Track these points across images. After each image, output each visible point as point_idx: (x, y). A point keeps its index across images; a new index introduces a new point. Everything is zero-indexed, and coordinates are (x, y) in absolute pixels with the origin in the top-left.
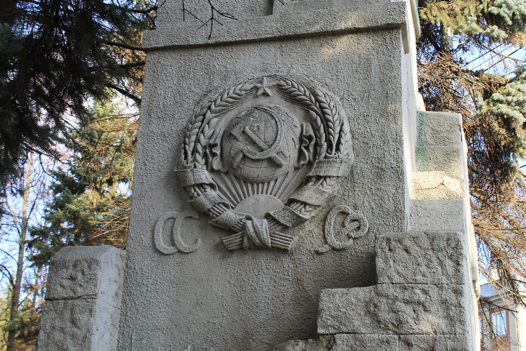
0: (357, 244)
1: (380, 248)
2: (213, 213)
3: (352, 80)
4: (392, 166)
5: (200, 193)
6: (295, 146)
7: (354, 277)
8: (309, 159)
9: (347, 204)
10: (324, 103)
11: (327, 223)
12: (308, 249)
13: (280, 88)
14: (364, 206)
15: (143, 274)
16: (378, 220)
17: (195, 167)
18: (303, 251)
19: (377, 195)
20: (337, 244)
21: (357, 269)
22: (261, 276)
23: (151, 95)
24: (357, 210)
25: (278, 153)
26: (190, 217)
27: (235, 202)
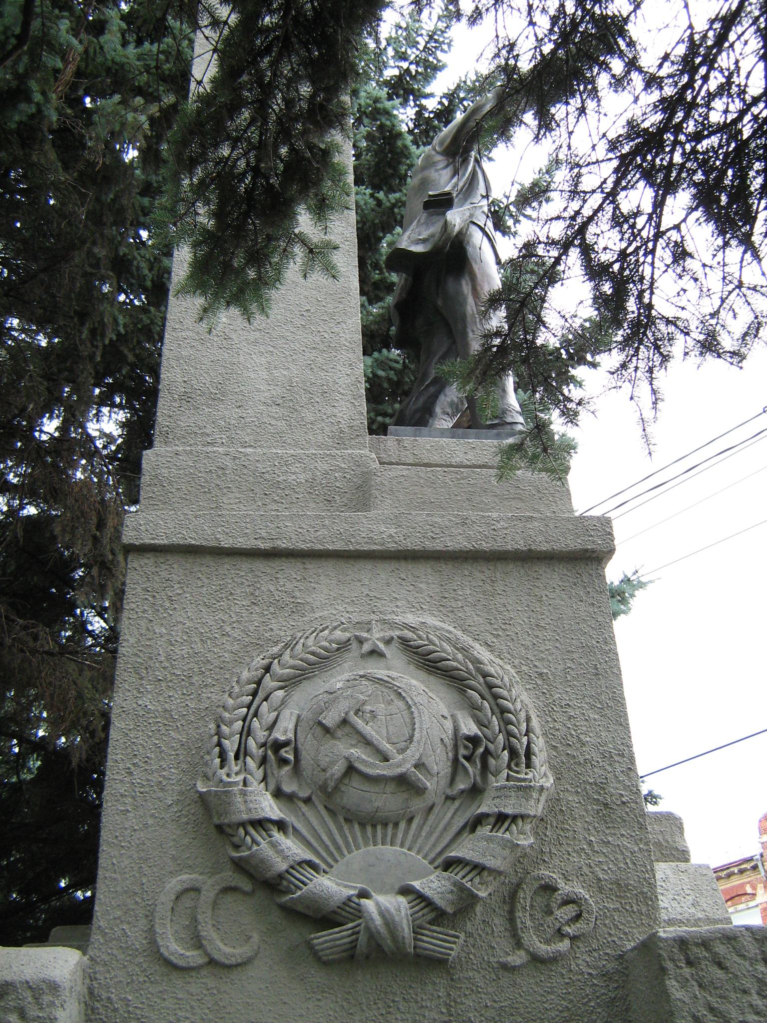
0: (579, 948)
2: (291, 882)
4: (623, 799)
5: (259, 839)
7: (579, 1015)
10: (493, 677)
12: (486, 958)
14: (582, 875)
15: (129, 1012)
17: (245, 783)
20: (544, 949)
21: (583, 998)
22: (394, 1017)
27: (330, 860)
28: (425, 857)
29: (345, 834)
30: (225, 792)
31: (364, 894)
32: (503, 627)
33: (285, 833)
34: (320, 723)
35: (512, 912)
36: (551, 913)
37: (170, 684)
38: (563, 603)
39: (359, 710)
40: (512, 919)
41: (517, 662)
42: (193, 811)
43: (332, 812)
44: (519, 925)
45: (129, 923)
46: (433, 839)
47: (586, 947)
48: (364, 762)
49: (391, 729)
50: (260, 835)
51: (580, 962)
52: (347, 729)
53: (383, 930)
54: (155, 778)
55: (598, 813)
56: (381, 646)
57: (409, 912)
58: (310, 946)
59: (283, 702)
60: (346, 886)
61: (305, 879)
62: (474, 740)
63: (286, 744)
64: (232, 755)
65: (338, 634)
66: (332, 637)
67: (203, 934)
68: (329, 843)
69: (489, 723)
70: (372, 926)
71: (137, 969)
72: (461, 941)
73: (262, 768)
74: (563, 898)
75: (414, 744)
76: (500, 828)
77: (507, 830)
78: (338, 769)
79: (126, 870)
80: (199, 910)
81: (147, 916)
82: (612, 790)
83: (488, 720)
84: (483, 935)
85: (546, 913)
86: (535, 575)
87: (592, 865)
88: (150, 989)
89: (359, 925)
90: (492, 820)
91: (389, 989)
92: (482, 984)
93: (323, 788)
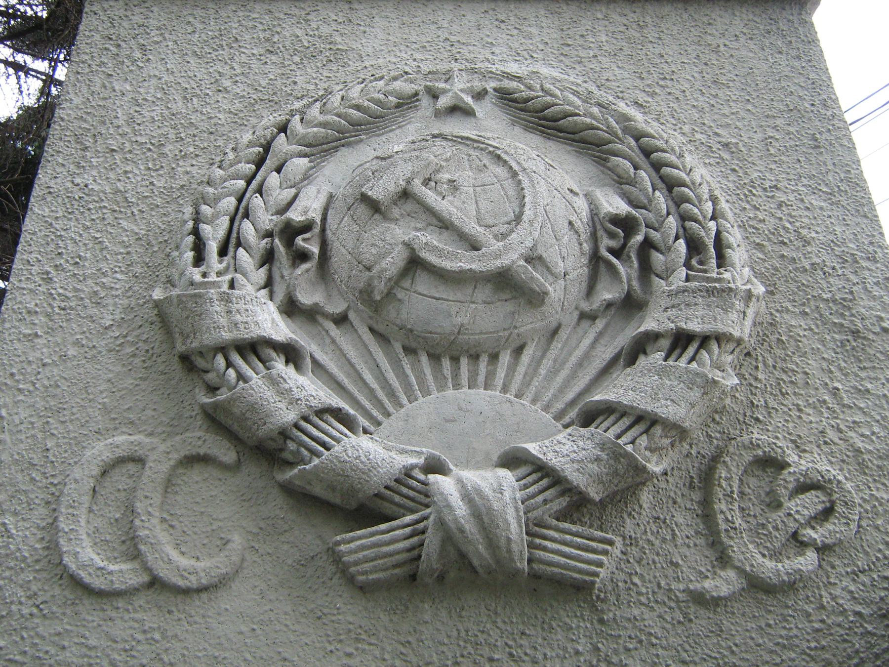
0: (833, 567)
2: (302, 444)
5: (249, 372)
6: (581, 244)
8: (630, 285)
9: (770, 434)
12: (663, 583)
13: (506, 98)
14: (826, 443)
17: (232, 285)
18: (644, 590)
19: (860, 409)
21: (850, 657)
24: (807, 455)
25: (528, 260)
26: (203, 460)
27: (375, 413)
28: (546, 408)
29: (404, 373)
30: (195, 295)
31: (435, 467)
32: (661, 83)
33: (298, 368)
34: (365, 198)
35: (706, 503)
36: (779, 505)
37: (128, 156)
38: (752, 55)
39: (430, 179)
40: (707, 515)
41: (686, 128)
42: (145, 336)
43: (382, 338)
44: (723, 526)
45: (15, 514)
46: (559, 379)
47: (848, 565)
48: (434, 249)
49: (483, 205)
50: (253, 369)
51: (838, 592)
52: (409, 206)
53: (470, 527)
54: (89, 286)
55: (843, 345)
56: (468, 100)
57: (518, 495)
58: (336, 558)
59: (307, 177)
60: (403, 452)
61: (327, 439)
62: (626, 224)
63: (306, 227)
64: (213, 247)
65: (398, 85)
66: (390, 88)
67: (142, 533)
68: (375, 385)
69: (650, 201)
70: (448, 518)
71: (21, 593)
72: (616, 551)
73: (266, 267)
74: (797, 480)
75: (525, 224)
76: (680, 356)
77: (693, 359)
78: (393, 262)
79: (21, 427)
80: (140, 494)
81: (48, 503)
82: (863, 311)
83: (647, 195)
84: (657, 543)
85: (768, 505)
86: (705, 19)
87: (842, 427)
88: (40, 630)
89: (426, 518)
90: (665, 343)
91: (481, 638)
92: (656, 630)
93: (366, 294)
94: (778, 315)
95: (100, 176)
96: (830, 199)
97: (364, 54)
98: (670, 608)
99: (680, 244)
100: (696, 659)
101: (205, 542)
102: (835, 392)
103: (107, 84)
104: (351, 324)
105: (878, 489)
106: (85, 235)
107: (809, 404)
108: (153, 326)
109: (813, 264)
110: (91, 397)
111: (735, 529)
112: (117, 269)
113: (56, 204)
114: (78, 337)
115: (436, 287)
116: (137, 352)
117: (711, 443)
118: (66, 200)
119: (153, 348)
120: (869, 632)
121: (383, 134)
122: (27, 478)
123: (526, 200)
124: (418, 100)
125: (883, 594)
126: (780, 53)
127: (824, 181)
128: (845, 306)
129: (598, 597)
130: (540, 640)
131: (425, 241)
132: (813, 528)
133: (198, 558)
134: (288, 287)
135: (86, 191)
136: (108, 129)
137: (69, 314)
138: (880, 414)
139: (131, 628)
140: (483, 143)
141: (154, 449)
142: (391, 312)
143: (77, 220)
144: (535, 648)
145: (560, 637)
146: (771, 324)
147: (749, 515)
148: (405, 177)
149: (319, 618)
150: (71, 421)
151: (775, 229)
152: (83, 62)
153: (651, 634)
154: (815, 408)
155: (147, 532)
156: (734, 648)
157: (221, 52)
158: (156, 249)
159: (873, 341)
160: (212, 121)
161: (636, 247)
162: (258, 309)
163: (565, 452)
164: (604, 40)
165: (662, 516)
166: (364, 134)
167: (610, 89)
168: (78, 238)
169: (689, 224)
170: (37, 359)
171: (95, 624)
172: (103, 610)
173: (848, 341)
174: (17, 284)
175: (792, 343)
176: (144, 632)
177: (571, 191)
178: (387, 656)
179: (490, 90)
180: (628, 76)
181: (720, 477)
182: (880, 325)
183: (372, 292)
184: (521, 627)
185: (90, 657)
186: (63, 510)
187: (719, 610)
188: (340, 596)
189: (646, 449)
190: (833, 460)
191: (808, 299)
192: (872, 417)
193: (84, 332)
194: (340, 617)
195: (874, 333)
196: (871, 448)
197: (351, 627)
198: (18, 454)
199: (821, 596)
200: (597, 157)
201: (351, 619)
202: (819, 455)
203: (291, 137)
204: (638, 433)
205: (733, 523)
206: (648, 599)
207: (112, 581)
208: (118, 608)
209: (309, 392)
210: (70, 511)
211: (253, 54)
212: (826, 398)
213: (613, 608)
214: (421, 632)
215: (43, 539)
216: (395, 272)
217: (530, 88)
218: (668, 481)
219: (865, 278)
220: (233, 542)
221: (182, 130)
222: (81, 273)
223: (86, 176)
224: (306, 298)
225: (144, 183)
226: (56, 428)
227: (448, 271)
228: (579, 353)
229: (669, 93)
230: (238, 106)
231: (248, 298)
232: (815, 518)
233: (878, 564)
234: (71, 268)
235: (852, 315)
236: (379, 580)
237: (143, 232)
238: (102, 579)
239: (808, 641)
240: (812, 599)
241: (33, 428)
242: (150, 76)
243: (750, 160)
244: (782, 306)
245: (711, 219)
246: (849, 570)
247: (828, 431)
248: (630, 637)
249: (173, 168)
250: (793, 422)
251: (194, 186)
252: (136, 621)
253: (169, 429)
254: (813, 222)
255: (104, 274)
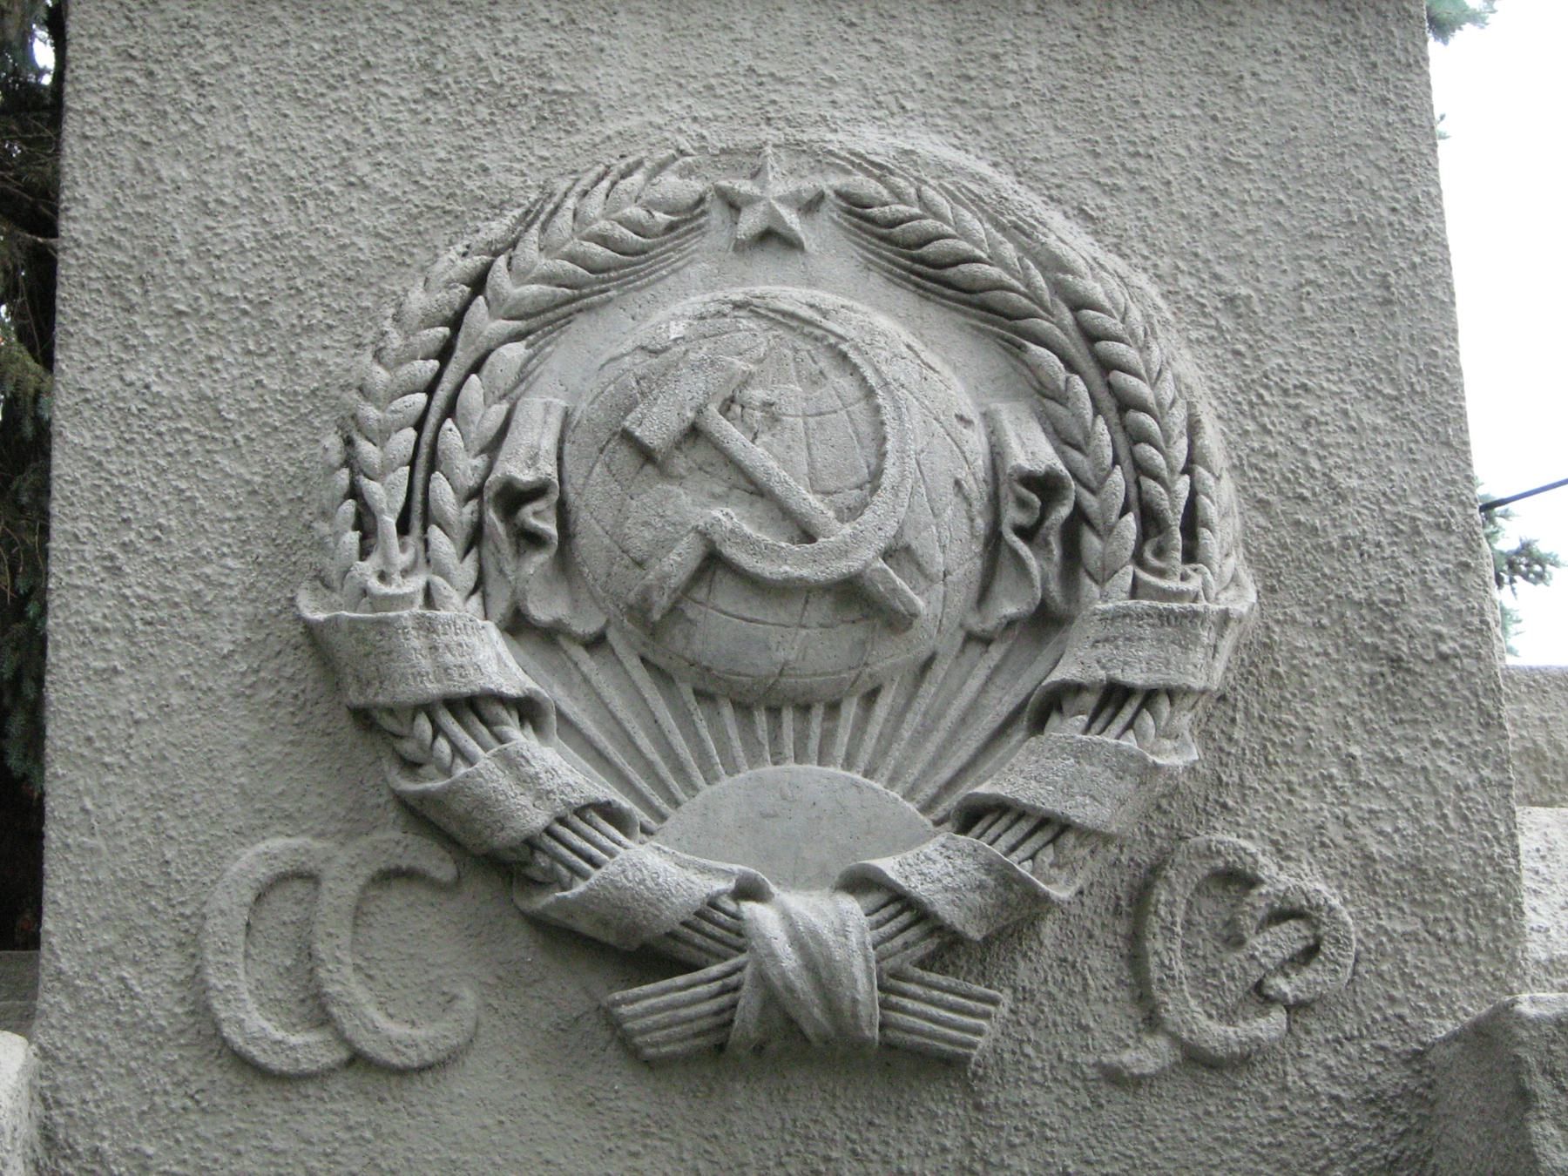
0: (1308, 1032)
1: (1544, 1072)
3: (1208, 200)
4: (1444, 648)
5: (472, 746)
6: (972, 520)
8: (1045, 589)
9: (1240, 830)
10: (1100, 309)
11: (1154, 924)
14: (1323, 844)
16: (1394, 912)
18: (1039, 1064)
19: (1383, 789)
20: (1216, 1033)
21: (1315, 1158)
23: (121, 185)
24: (1292, 865)
25: (887, 555)
27: (658, 801)
28: (909, 795)
29: (697, 734)
30: (379, 622)
31: (749, 891)
32: (1131, 164)
33: (538, 729)
34: (627, 437)
35: (1136, 938)
37: (210, 324)
38: (1298, 96)
39: (732, 400)
40: (1135, 958)
41: (1165, 264)
42: (289, 671)
43: (662, 676)
44: (1155, 974)
45: (135, 962)
46: (931, 747)
47: (1330, 1029)
50: (475, 737)
51: (1310, 1067)
52: (701, 453)
53: (802, 984)
54: (183, 582)
55: (1373, 683)
58: (613, 1023)
59: (524, 376)
60: (703, 870)
61: (594, 851)
62: (1045, 486)
63: (537, 492)
64: (389, 521)
67: (332, 989)
68: (654, 755)
70: (773, 973)
71: (164, 1079)
74: (1271, 906)
75: (884, 495)
76: (1110, 722)
77: (1130, 726)
78: (680, 559)
79: (120, 827)
80: (319, 930)
81: (181, 945)
82: (1414, 622)
84: (1061, 996)
85: (1226, 941)
87: (1352, 819)
88: (201, 1129)
89: (739, 969)
90: (1090, 700)
94: (1277, 629)
95: (168, 367)
96: (1394, 409)
97: (603, 104)
98: (1074, 1088)
99: (1127, 526)
100: (1105, 1158)
101: (421, 999)
102: (1349, 763)
103: (145, 165)
104: (613, 651)
105: (1390, 917)
106: (162, 485)
107: (1307, 781)
108: (299, 653)
109: (1345, 538)
110: (220, 774)
111: (1173, 978)
112: (225, 550)
113: (100, 423)
114: (183, 672)
115: (746, 600)
116: (280, 697)
117: (1152, 842)
118: (117, 415)
119: (303, 691)
120: (1347, 1124)
121: (647, 285)
122: (143, 908)
123: (888, 429)
124: (704, 213)
125: (1373, 1071)
126: (1353, 90)
127: (1388, 373)
128: (1385, 614)
129: (975, 1074)
130: (894, 1132)
131: (729, 526)
132: (1287, 976)
133: (413, 1024)
134: (514, 593)
135: (148, 397)
136: (163, 264)
137: (161, 632)
138: (1411, 798)
139: (329, 1123)
140: (819, 327)
141: (328, 859)
142: (676, 638)
143: (142, 454)
144: (887, 1144)
145: (920, 1128)
146: (1265, 645)
147: (1196, 955)
148: (693, 404)
149: (591, 1105)
150: (196, 815)
151: (1293, 472)
152: (91, 113)
153: (1044, 1124)
154: (1315, 786)
155: (338, 988)
156: (1158, 1144)
157: (344, 94)
158: (284, 512)
159: (1422, 675)
160: (348, 254)
161: (1057, 528)
162: (475, 640)
163: (936, 875)
164: (1033, 66)
165: (1070, 958)
166: (618, 287)
167: (1038, 180)
168: (150, 490)
169: (1149, 484)
170: (124, 712)
171: (278, 1119)
172: (287, 1099)
173: (1382, 675)
174: (66, 579)
175: (1295, 676)
176: (350, 1129)
177: (961, 418)
178: (686, 1156)
179: (830, 193)
180: (1072, 149)
181: (1158, 901)
182: (1436, 648)
183: (650, 610)
184: (868, 1115)
185: (277, 1165)
186: (210, 957)
187: (1141, 1091)
188: (619, 1074)
189: (1051, 865)
190: (1330, 872)
191: (1328, 602)
192: (1399, 803)
193: (190, 664)
194: (620, 1103)
195: (1425, 661)
196: (1390, 854)
197: (636, 1116)
198: (123, 869)
199: (1286, 1074)
200: (1007, 341)
201: (636, 1106)
202: (1310, 864)
203: (494, 305)
204: (1041, 843)
205: (1171, 969)
206: (1044, 1076)
207: (297, 1060)
208: (308, 1096)
209: (565, 779)
210: (221, 958)
211: (402, 99)
212: (1334, 771)
213: (994, 1090)
214: (732, 1123)
215: (183, 999)
216: (684, 578)
217: (899, 196)
218: (1082, 904)
219: (1426, 563)
220: (463, 999)
221: (296, 270)
222: (166, 556)
223: (142, 367)
224: (542, 611)
225: (245, 382)
226: (174, 827)
227: (765, 579)
228: (962, 701)
229: (1142, 189)
230: (388, 220)
231: (460, 623)
232: (1292, 960)
233: (1374, 1029)
234: (148, 548)
235: (1395, 630)
236: (674, 1053)
237: (258, 479)
238: (283, 1057)
239: (1261, 1135)
240: (1273, 1077)
241: (139, 828)
242: (220, 148)
243: (1267, 330)
244: (1285, 614)
245: (1184, 472)
246: (1330, 1036)
247: (1329, 825)
248: (1016, 1129)
249: (292, 353)
250: (1279, 810)
251: (335, 392)
252: (336, 1114)
253: (347, 826)
254: (1358, 457)
255: (207, 560)
